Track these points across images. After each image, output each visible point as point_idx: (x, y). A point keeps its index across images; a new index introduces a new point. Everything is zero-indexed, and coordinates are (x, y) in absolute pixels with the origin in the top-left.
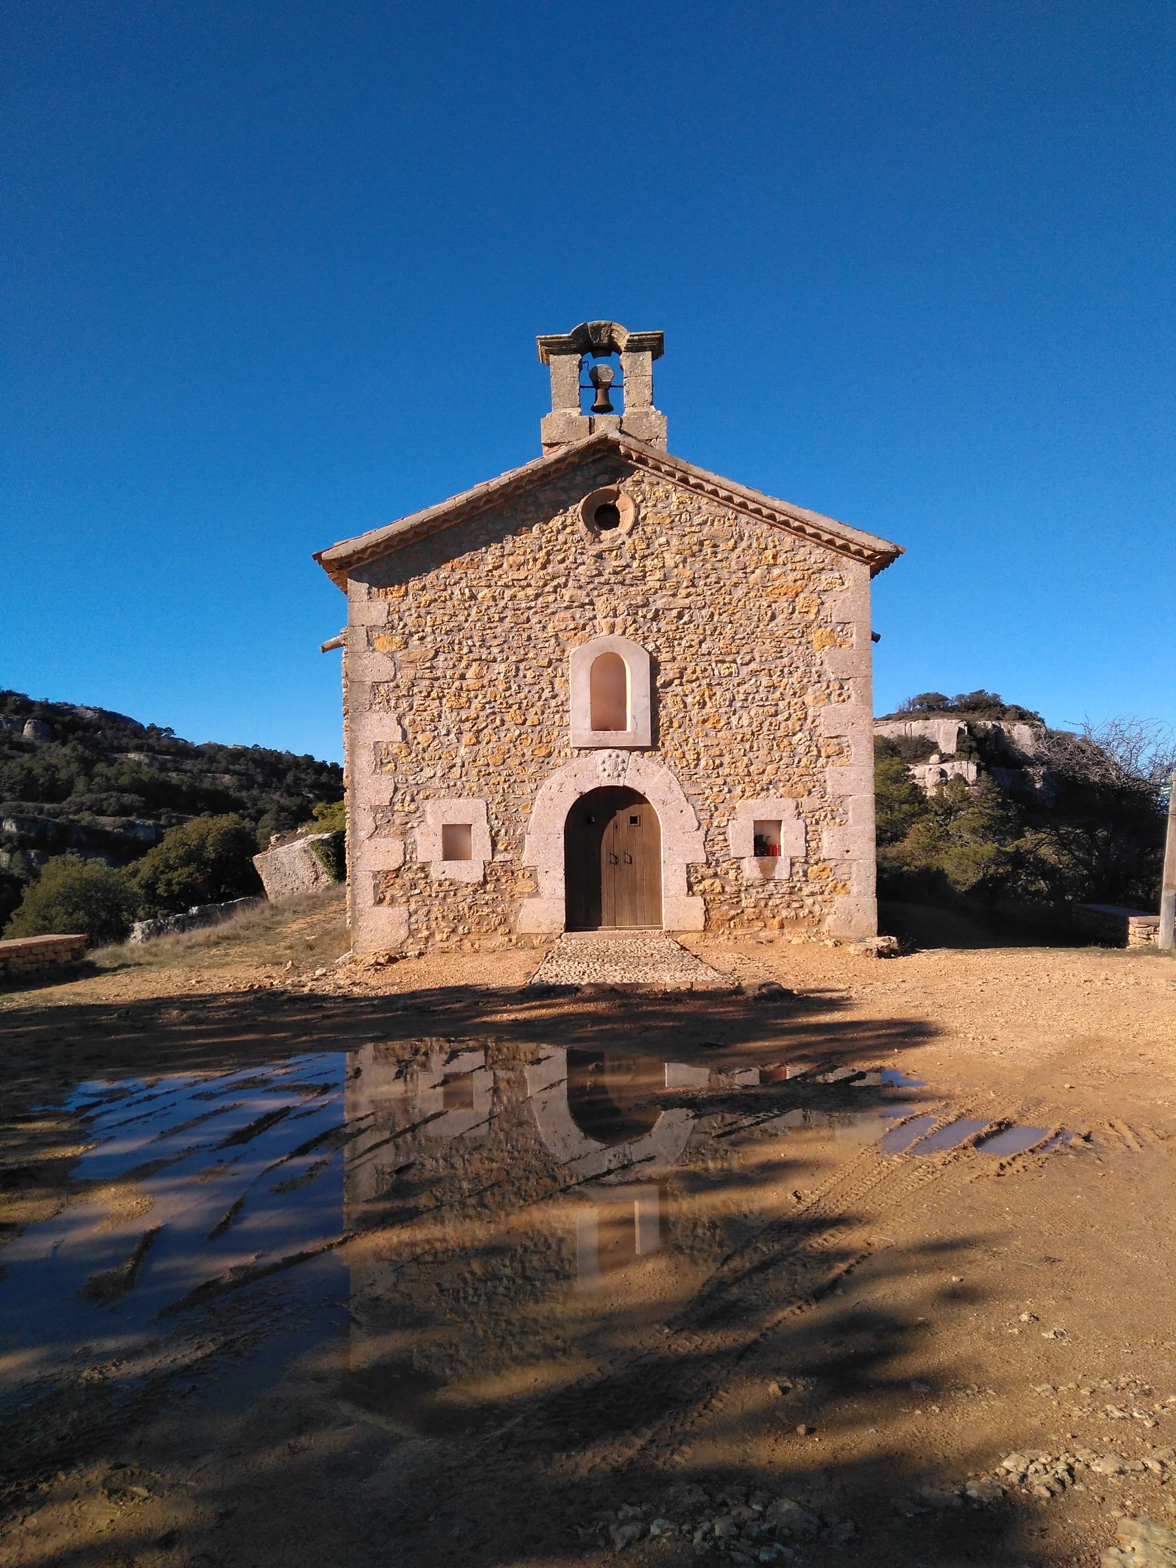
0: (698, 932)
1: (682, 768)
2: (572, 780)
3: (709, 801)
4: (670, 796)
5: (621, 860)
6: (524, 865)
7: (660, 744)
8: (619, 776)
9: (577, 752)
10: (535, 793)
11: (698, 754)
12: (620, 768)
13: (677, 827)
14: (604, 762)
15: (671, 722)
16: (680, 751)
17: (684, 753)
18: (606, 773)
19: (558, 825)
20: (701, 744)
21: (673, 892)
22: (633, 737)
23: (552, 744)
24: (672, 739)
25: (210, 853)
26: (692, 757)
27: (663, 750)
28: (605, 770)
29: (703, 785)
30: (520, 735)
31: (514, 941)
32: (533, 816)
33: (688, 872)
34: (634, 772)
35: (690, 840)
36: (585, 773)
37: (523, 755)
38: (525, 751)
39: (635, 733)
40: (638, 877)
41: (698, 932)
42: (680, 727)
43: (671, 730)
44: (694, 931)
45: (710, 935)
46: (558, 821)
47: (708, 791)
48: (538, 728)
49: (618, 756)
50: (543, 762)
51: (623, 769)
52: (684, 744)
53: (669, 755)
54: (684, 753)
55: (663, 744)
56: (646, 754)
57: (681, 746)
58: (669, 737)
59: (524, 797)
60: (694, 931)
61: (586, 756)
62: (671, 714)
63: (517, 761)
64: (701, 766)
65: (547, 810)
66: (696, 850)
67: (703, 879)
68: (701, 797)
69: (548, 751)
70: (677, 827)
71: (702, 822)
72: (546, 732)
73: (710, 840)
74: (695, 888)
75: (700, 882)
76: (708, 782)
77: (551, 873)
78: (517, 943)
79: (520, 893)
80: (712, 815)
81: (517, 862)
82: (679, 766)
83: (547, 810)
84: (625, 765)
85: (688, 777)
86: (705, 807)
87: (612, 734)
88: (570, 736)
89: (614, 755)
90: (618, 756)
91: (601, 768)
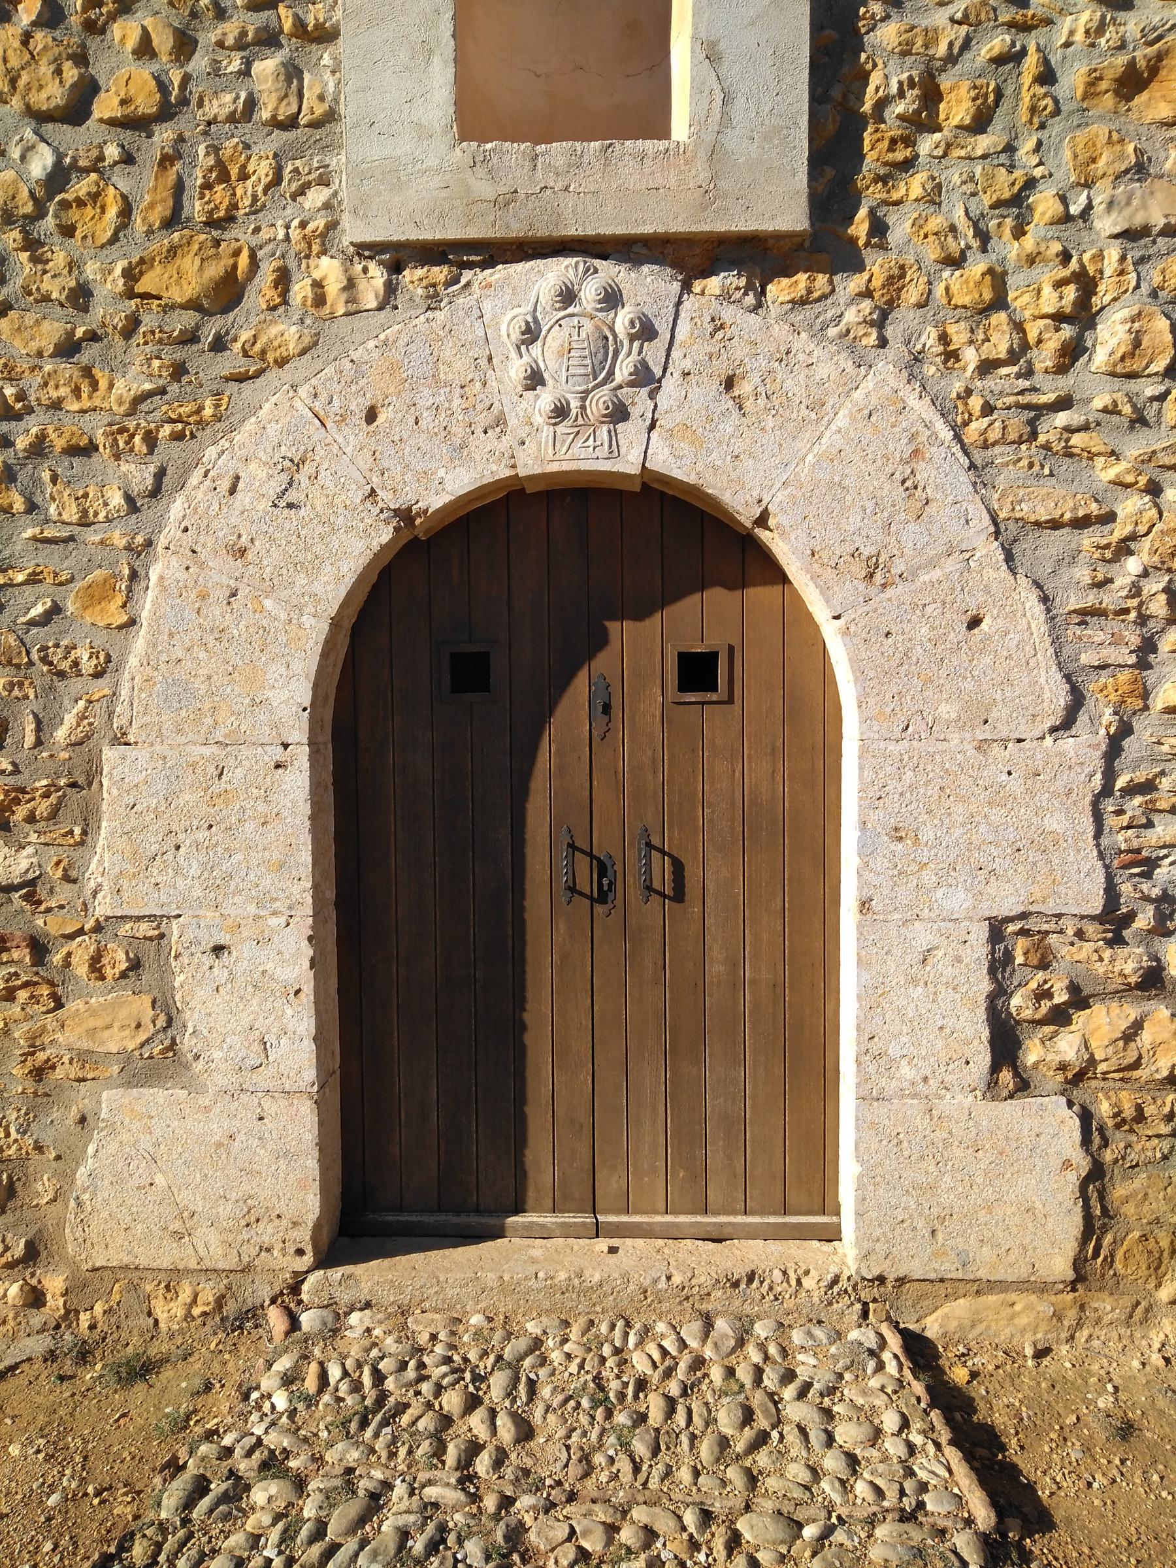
0: (1043, 1288)
1: (987, 367)
2: (353, 437)
3: (1133, 565)
4: (910, 535)
5: (630, 888)
6: (103, 907)
7: (860, 228)
8: (619, 414)
9: (377, 275)
10: (149, 514)
11: (1086, 283)
12: (623, 370)
13: (947, 711)
14: (531, 334)
15: (931, 96)
16: (977, 267)
17: (997, 278)
18: (545, 399)
19: (276, 697)
20: (1106, 224)
21: (906, 1071)
22: (700, 173)
23: (240, 234)
24: (934, 196)
25: (763, 535)
26: (1049, 302)
27: (877, 266)
28: (535, 380)
29: (1109, 473)
30: (58, 178)
31: (55, 1303)
32: (139, 643)
33: (999, 965)
34: (705, 391)
35: (1015, 785)
36: (425, 398)
37: (81, 296)
38: (91, 270)
39: (714, 154)
40: (716, 968)
41: (1043, 1288)
42: (980, 123)
43: (927, 144)
44: (1023, 1286)
45: (1105, 1305)
46: (276, 671)
47: (1130, 506)
48: (164, 135)
49: (612, 299)
50: (190, 338)
51: (644, 377)
52: (1002, 226)
53: (912, 295)
54: (997, 278)
55: (879, 228)
56: (779, 290)
57: (984, 237)
58: (915, 185)
59: (93, 536)
60: (1023, 1286)
61: (433, 300)
62: (931, 38)
63: (50, 332)
64: (1100, 358)
65: (216, 611)
66: (1047, 843)
67: (1079, 999)
68: (1088, 539)
69: (215, 270)
70: (947, 711)
71: (1092, 685)
72: (204, 160)
73: (1132, 790)
74: (1032, 1053)
75: (1060, 1017)
76: (1135, 446)
77: (244, 954)
78: (70, 1313)
79: (83, 1057)
80: (1148, 646)
81: (64, 893)
82: (971, 357)
83: (216, 611)
84: (654, 353)
85: (1017, 423)
86: (1110, 599)
87: (576, 163)
88: (342, 184)
89: (589, 293)
90: (612, 299)
91: (517, 369)
